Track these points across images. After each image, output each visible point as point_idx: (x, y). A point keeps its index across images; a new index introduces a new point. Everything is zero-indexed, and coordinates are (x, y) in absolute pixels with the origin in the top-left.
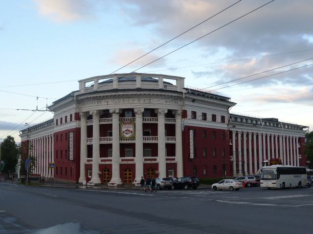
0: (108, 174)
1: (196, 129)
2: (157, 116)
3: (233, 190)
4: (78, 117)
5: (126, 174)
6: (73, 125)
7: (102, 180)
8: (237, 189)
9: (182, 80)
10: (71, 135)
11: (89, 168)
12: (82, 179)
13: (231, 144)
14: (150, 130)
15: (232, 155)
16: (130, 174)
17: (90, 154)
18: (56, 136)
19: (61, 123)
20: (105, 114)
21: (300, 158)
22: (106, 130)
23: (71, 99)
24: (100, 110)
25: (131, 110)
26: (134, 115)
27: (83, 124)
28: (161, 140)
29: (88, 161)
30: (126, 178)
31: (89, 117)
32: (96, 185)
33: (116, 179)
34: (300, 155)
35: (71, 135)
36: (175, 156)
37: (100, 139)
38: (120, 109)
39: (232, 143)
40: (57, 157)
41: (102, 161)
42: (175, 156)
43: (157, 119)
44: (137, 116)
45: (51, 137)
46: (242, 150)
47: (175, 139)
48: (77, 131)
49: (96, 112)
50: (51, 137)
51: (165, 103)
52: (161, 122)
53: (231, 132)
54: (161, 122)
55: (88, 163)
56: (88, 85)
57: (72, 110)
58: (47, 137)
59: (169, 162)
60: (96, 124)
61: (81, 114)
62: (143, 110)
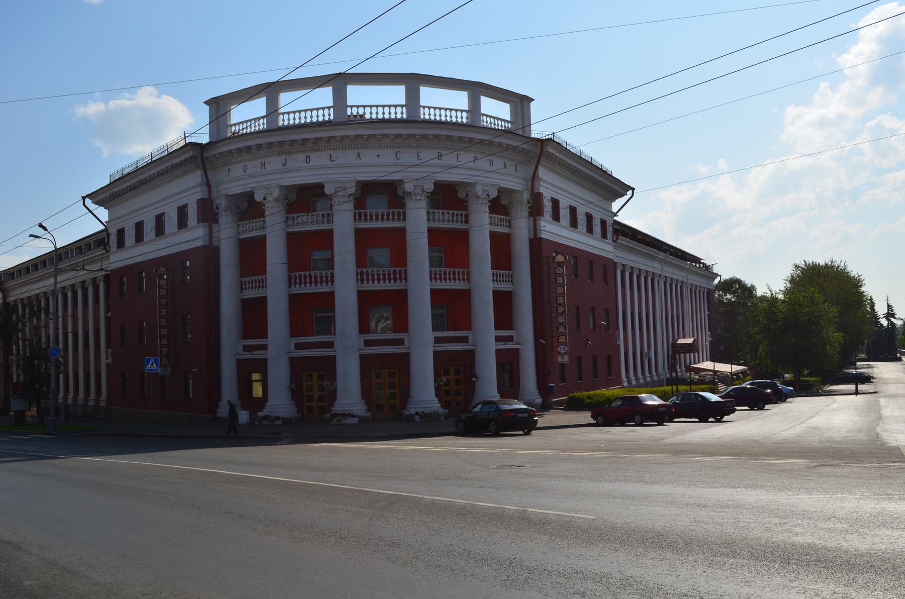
2: (466, 208)
4: (208, 212)
6: (194, 236)
9: (525, 103)
15: (108, 365)
17: (504, 303)
20: (305, 198)
21: (110, 360)
22: (308, 250)
24: (288, 188)
27: (227, 234)
28: (484, 282)
30: (392, 386)
36: (264, 335)
37: (290, 278)
41: (247, 348)
42: (468, 327)
43: (404, 213)
44: (410, 204)
46: (647, 315)
47: (263, 284)
48: (209, 255)
49: (276, 193)
51: (436, 161)
52: (418, 220)
54: (418, 220)
55: (247, 356)
57: (188, 189)
59: (502, 346)
60: (274, 231)
61: (222, 202)
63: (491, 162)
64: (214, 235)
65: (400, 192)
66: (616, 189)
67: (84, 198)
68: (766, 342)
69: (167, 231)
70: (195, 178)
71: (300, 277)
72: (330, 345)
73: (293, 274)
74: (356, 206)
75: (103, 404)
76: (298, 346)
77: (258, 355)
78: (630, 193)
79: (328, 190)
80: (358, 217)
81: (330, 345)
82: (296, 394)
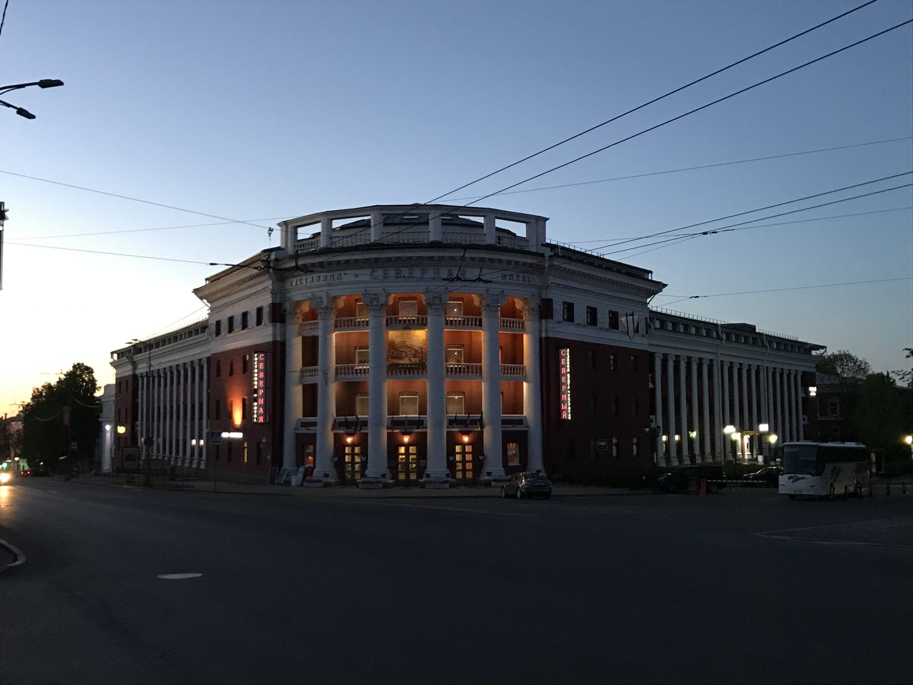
10: (257, 361)
21: (806, 422)
34: (806, 416)
35: (257, 361)
56: (304, 233)
69: (250, 326)
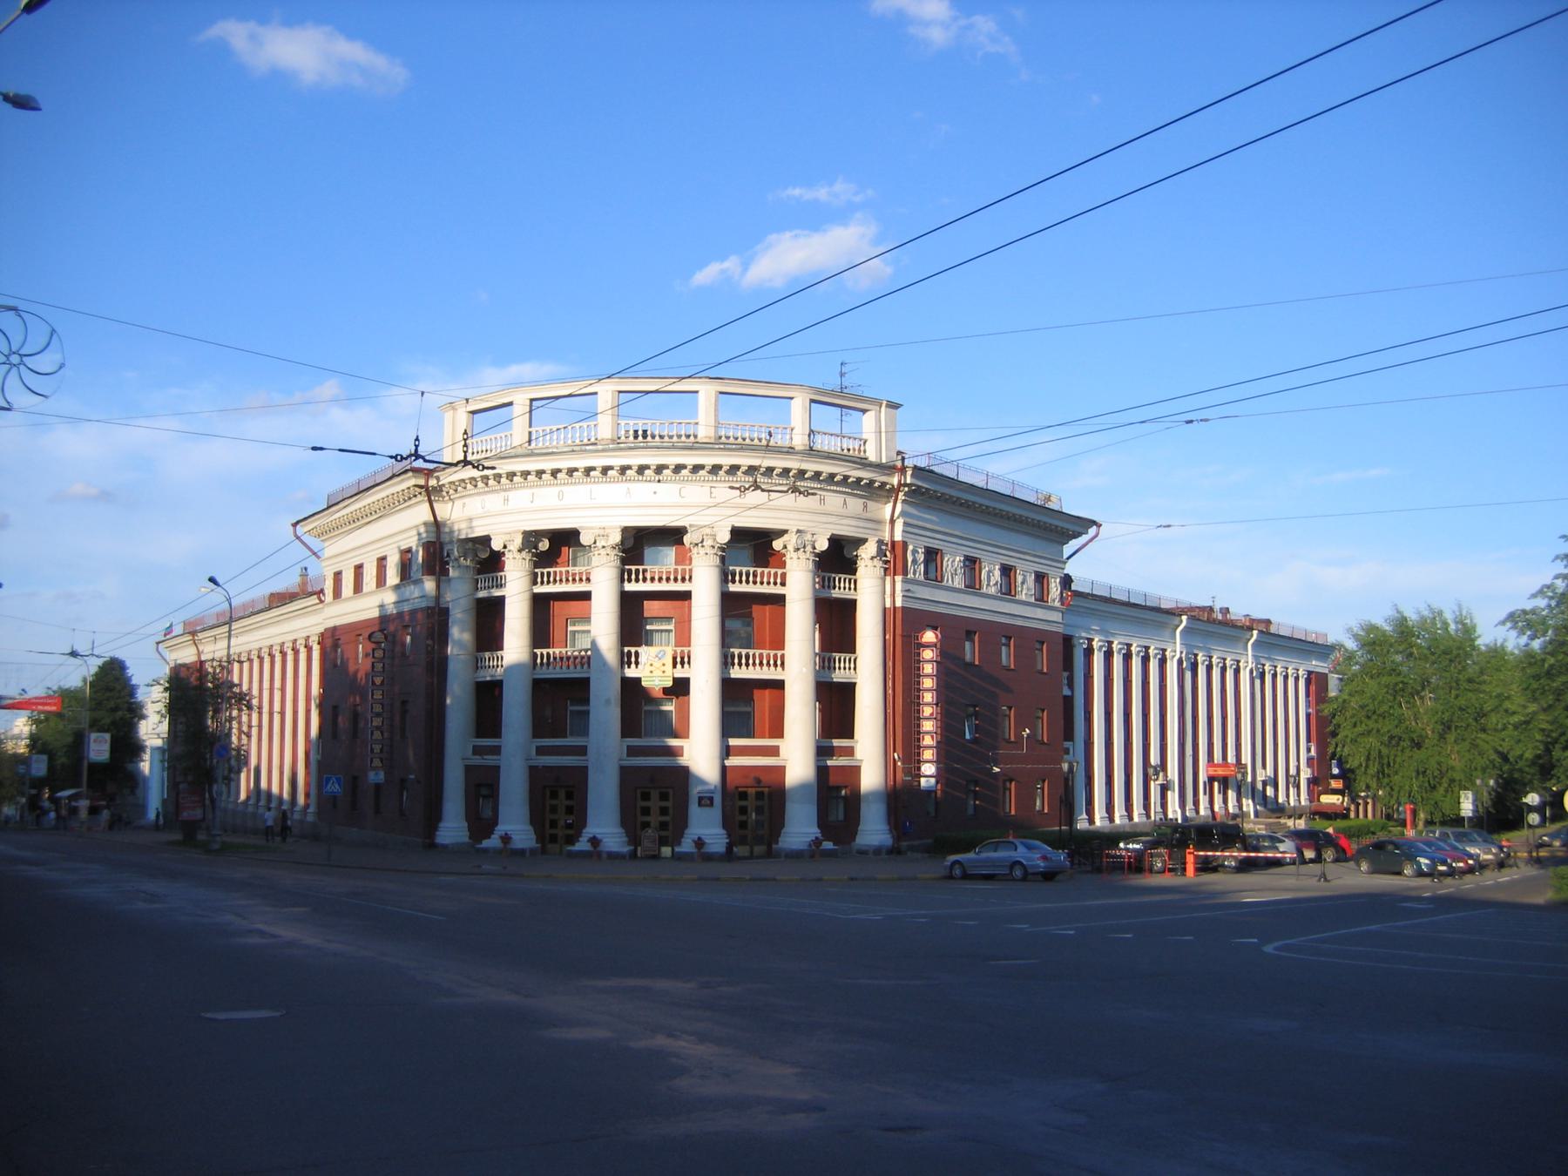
0: (569, 810)
1: (957, 630)
3: (1024, 879)
5: (759, 810)
7: (540, 837)
8: (1049, 876)
11: (483, 786)
12: (453, 828)
13: (1066, 692)
14: (747, 617)
16: (554, 809)
18: (329, 642)
19: (358, 587)
20: (555, 546)
23: (413, 482)
25: (672, 536)
26: (684, 558)
27: (459, 597)
29: (477, 751)
31: (489, 562)
32: (878, 851)
33: (604, 825)
38: (625, 530)
39: (1071, 686)
40: (335, 735)
43: (784, 576)
45: (309, 649)
46: (283, 689)
50: (309, 649)
52: (798, 586)
53: (1068, 641)
55: (477, 760)
58: (301, 642)
62: (724, 537)
63: (822, 501)
64: (215, 622)
65: (630, 543)
66: (1055, 528)
67: (295, 525)
68: (700, 751)
70: (818, 446)
71: (761, 656)
72: (582, 750)
73: (538, 651)
74: (624, 561)
75: (301, 799)
76: (541, 751)
77: (490, 760)
78: (1092, 531)
79: (585, 539)
80: (623, 576)
81: (582, 750)
82: (538, 818)
